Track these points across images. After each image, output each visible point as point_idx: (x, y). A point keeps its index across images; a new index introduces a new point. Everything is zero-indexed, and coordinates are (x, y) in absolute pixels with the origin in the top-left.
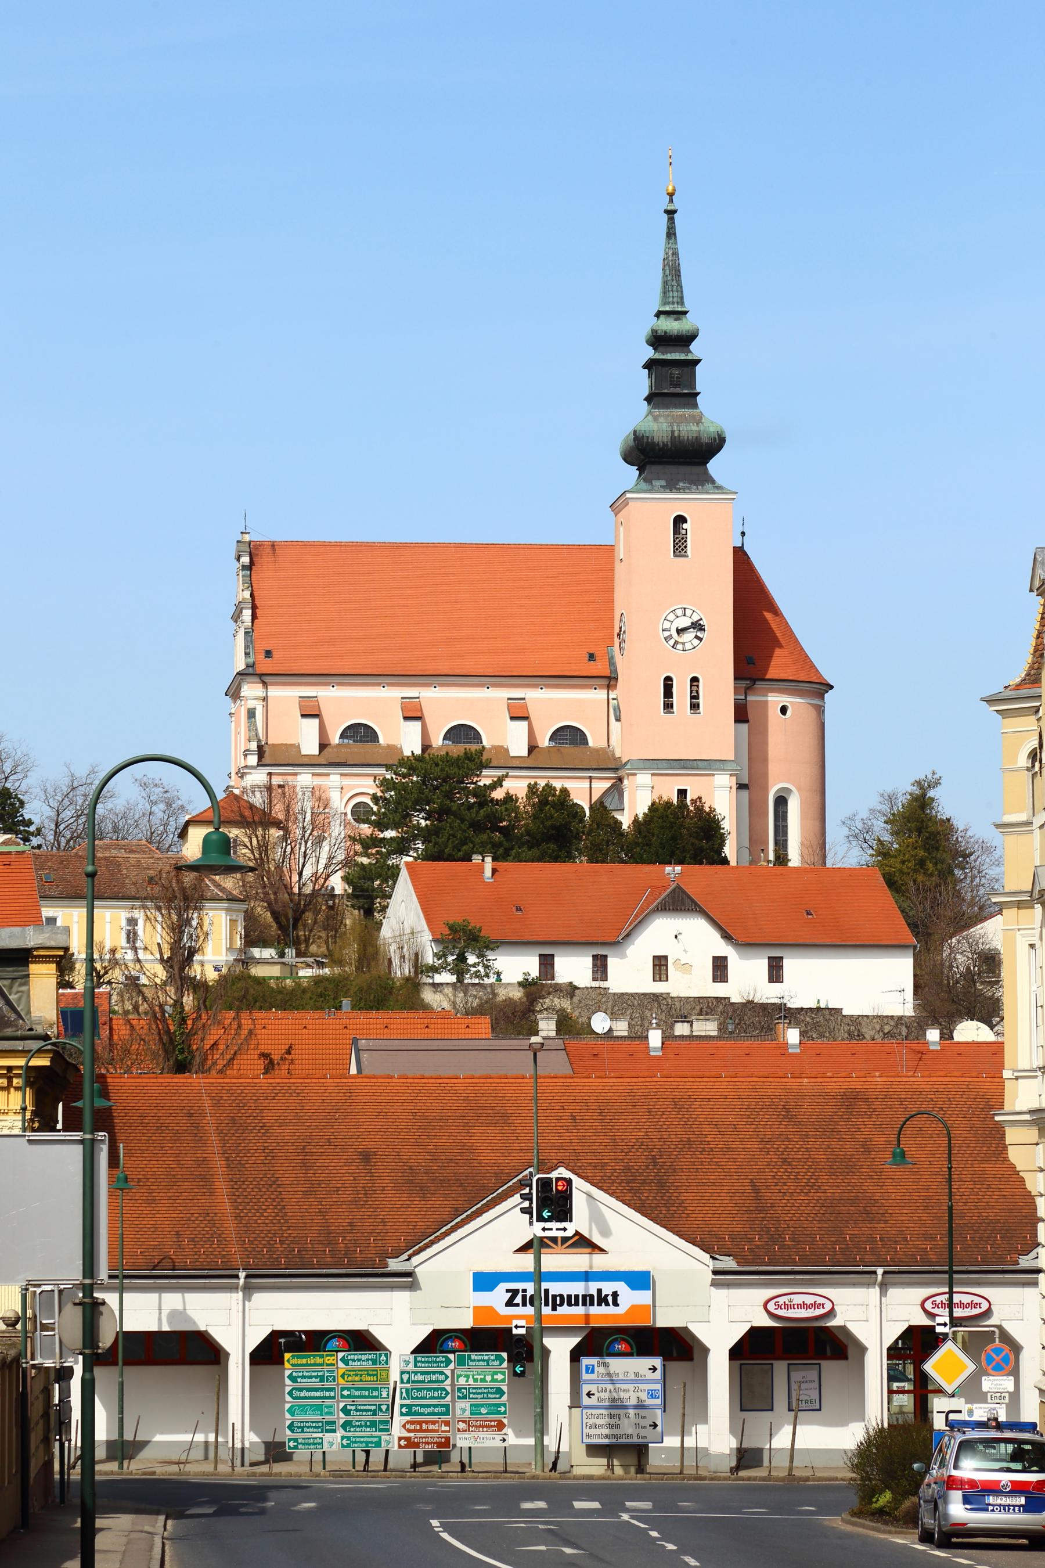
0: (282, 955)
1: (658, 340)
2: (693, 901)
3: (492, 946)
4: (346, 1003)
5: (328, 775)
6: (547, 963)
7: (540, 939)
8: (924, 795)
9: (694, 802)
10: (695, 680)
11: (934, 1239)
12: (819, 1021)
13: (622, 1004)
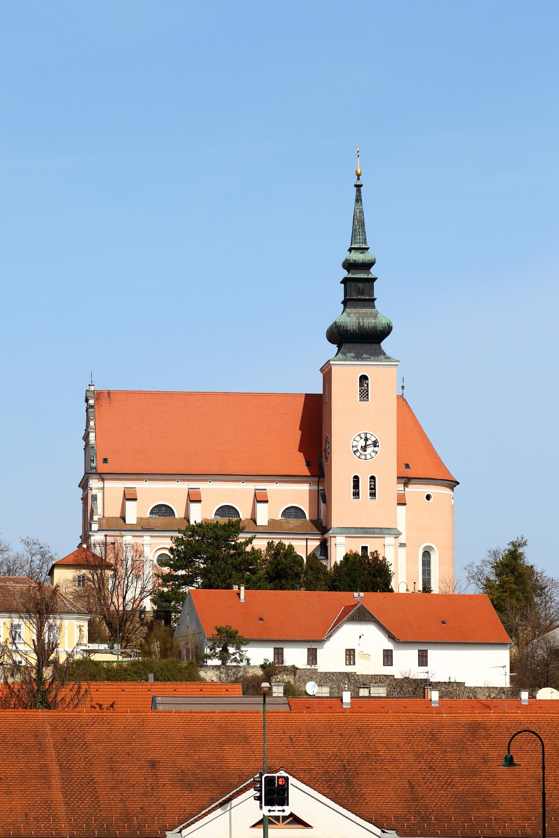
0: (112, 648)
1: (349, 266)
2: (371, 615)
3: (244, 642)
4: (151, 676)
5: (142, 536)
6: (279, 653)
7: (274, 638)
8: (516, 551)
9: (372, 554)
10: (373, 478)
11: (529, 819)
12: (451, 689)
13: (324, 678)
